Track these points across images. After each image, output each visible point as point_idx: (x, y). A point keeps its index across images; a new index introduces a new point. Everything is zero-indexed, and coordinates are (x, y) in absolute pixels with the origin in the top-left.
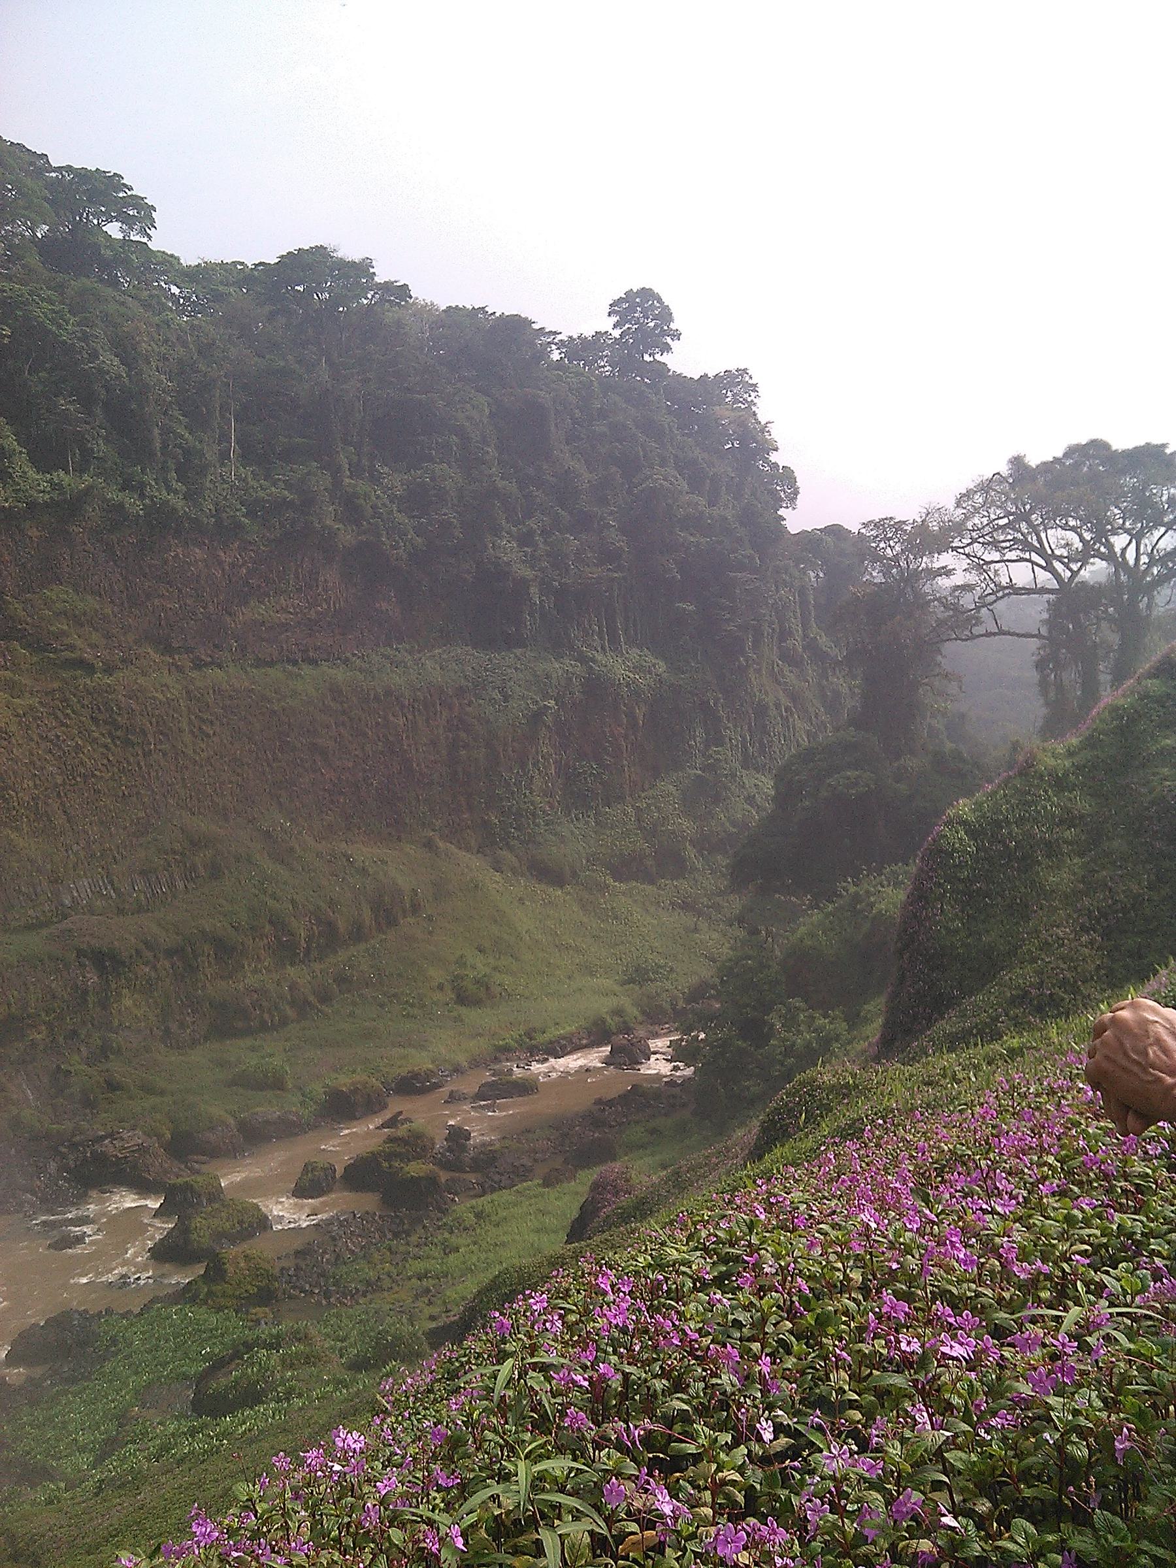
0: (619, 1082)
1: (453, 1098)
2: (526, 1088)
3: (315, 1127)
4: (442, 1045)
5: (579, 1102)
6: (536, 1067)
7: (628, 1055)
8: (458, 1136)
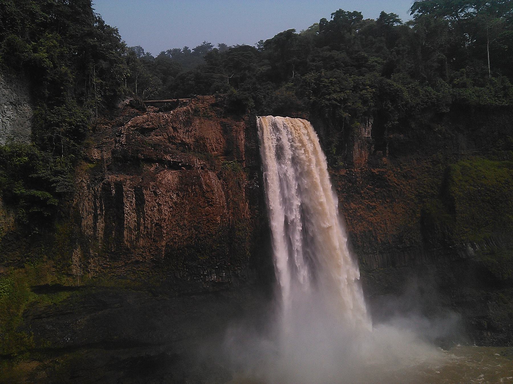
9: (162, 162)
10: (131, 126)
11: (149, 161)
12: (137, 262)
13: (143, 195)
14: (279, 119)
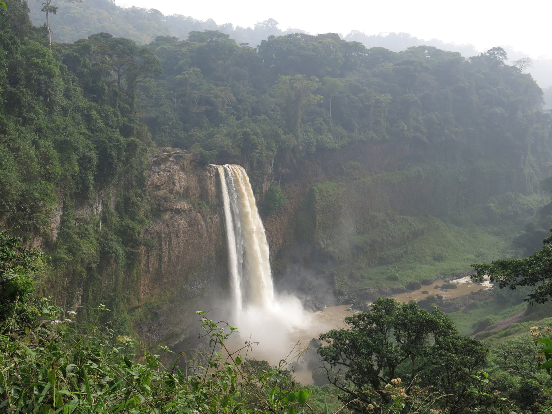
0: (475, 287)
1: (437, 287)
2: (453, 287)
3: (406, 291)
4: (425, 270)
5: (536, 322)
6: (455, 281)
8: (440, 298)
9: (172, 210)
10: (150, 185)
11: (166, 210)
12: (165, 282)
13: (171, 238)
14: (230, 168)
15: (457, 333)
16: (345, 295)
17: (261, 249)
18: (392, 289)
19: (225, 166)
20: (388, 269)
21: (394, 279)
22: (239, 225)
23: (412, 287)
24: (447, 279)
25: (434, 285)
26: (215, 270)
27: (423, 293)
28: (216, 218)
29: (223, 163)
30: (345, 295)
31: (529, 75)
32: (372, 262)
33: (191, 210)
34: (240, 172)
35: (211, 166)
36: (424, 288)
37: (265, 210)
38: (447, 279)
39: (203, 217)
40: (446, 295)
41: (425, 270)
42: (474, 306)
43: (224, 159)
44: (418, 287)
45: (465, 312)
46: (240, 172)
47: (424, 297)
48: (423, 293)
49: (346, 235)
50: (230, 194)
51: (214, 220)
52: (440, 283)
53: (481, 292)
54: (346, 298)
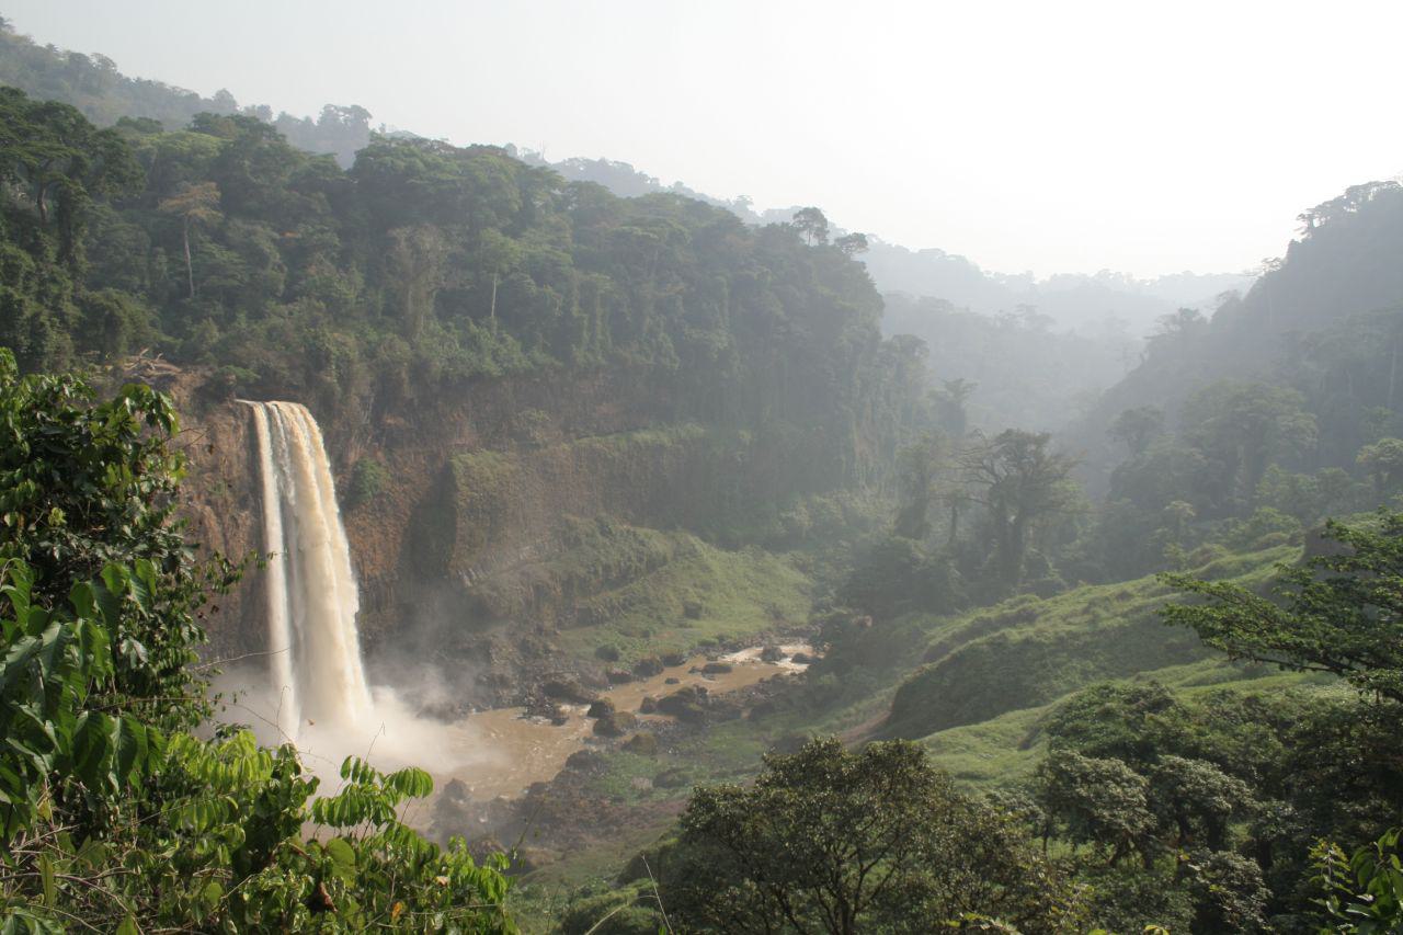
0: (766, 671)
1: (693, 671)
2: (726, 669)
3: (634, 679)
7: (771, 655)
8: (702, 691)
15: (297, 770)
16: (513, 687)
17: (342, 600)
18: (608, 674)
19: (270, 404)
20: (598, 634)
21: (612, 656)
22: (292, 494)
23: (646, 669)
24: (713, 654)
25: (688, 666)
26: (234, 611)
27: (670, 681)
28: (245, 516)
29: (264, 397)
30: (513, 687)
31: (863, 265)
32: (566, 619)
33: (191, 499)
34: (300, 422)
35: (237, 403)
36: (669, 672)
37: (350, 499)
38: (713, 654)
39: (218, 515)
40: (714, 685)
41: (666, 640)
42: (648, 727)
43: (268, 389)
44: (659, 671)
45: (752, 718)
46: (300, 416)
47: (672, 690)
48: (670, 681)
49: (510, 565)
50: (279, 468)
51: (240, 521)
52: (701, 662)
53: (778, 680)
54: (516, 692)
